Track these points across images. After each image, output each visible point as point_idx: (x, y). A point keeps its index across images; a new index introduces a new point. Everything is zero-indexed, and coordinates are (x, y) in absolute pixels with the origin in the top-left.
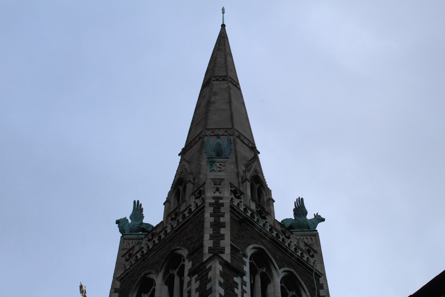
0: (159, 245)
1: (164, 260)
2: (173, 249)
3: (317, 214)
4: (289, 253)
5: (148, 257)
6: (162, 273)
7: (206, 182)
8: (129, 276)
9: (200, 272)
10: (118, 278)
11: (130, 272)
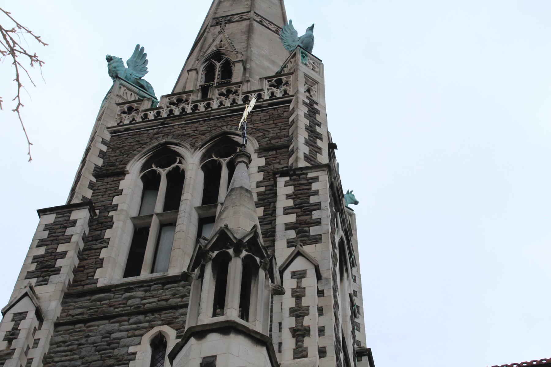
1: (208, 138)
2: (228, 130)
3: (352, 191)
4: (343, 217)
5: (171, 123)
6: (202, 152)
8: (131, 134)
9: (295, 177)
10: (108, 128)
11: (133, 130)
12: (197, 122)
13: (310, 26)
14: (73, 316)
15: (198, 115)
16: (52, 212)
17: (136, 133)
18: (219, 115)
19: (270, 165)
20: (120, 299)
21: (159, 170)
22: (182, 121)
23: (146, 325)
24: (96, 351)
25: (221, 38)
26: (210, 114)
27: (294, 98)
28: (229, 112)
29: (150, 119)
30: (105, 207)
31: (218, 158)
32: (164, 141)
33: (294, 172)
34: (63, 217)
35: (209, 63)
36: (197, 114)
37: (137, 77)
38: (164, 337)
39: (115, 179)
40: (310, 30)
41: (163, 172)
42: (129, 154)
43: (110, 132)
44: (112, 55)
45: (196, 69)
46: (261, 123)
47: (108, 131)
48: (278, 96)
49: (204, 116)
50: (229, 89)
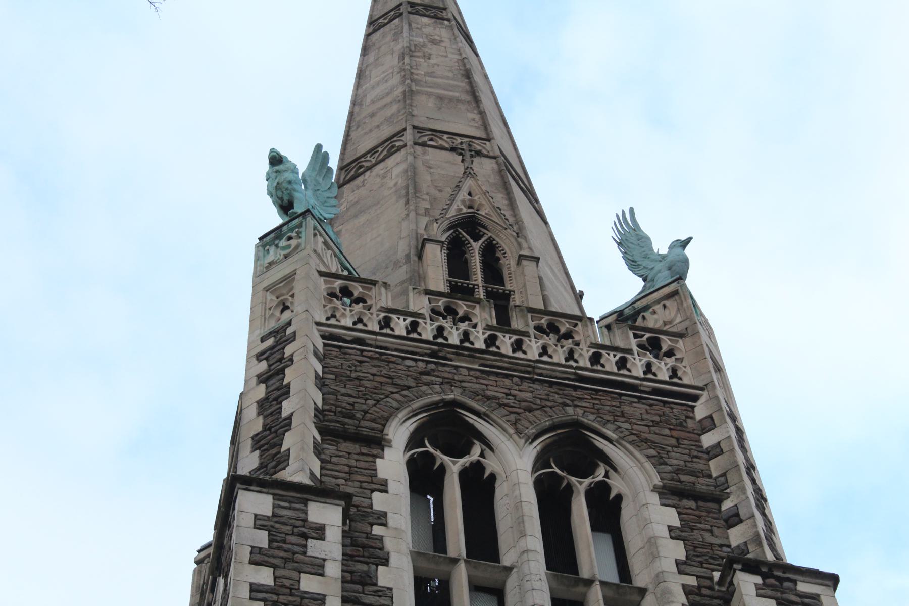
0: (506, 365)
1: (547, 423)
2: (585, 420)
5: (451, 360)
7: (455, 186)
8: (369, 354)
9: (771, 581)
11: (370, 346)
13: (683, 238)
15: (510, 363)
16: (264, 490)
17: (378, 356)
18: (551, 377)
21: (443, 458)
22: (472, 363)
25: (470, 187)
26: (534, 367)
27: (705, 394)
28: (572, 377)
30: (358, 510)
31: (563, 472)
32: (452, 396)
33: (770, 570)
34: (290, 508)
35: (454, 235)
36: (506, 359)
37: (321, 215)
39: (365, 450)
40: (681, 246)
41: (454, 467)
42: (378, 401)
43: (322, 333)
44: (283, 153)
45: (425, 239)
46: (644, 425)
47: (319, 331)
48: (660, 377)
49: (520, 368)
50: (554, 324)
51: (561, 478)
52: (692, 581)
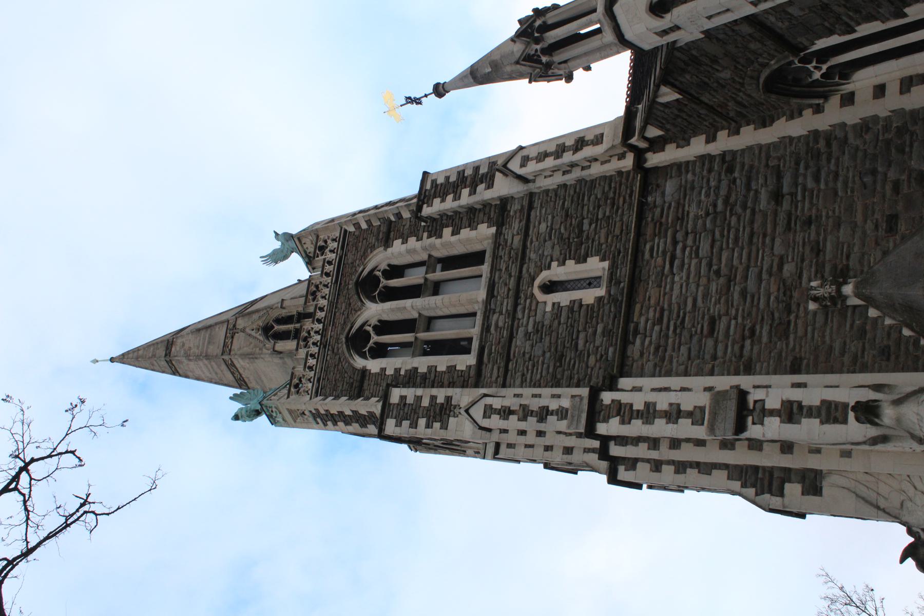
9: (426, 200)
12: (335, 314)
14: (498, 376)
19: (403, 234)
20: (495, 336)
22: (329, 330)
23: (528, 301)
24: (541, 342)
29: (317, 351)
38: (545, 284)
51: (380, 291)
52: (425, 235)
